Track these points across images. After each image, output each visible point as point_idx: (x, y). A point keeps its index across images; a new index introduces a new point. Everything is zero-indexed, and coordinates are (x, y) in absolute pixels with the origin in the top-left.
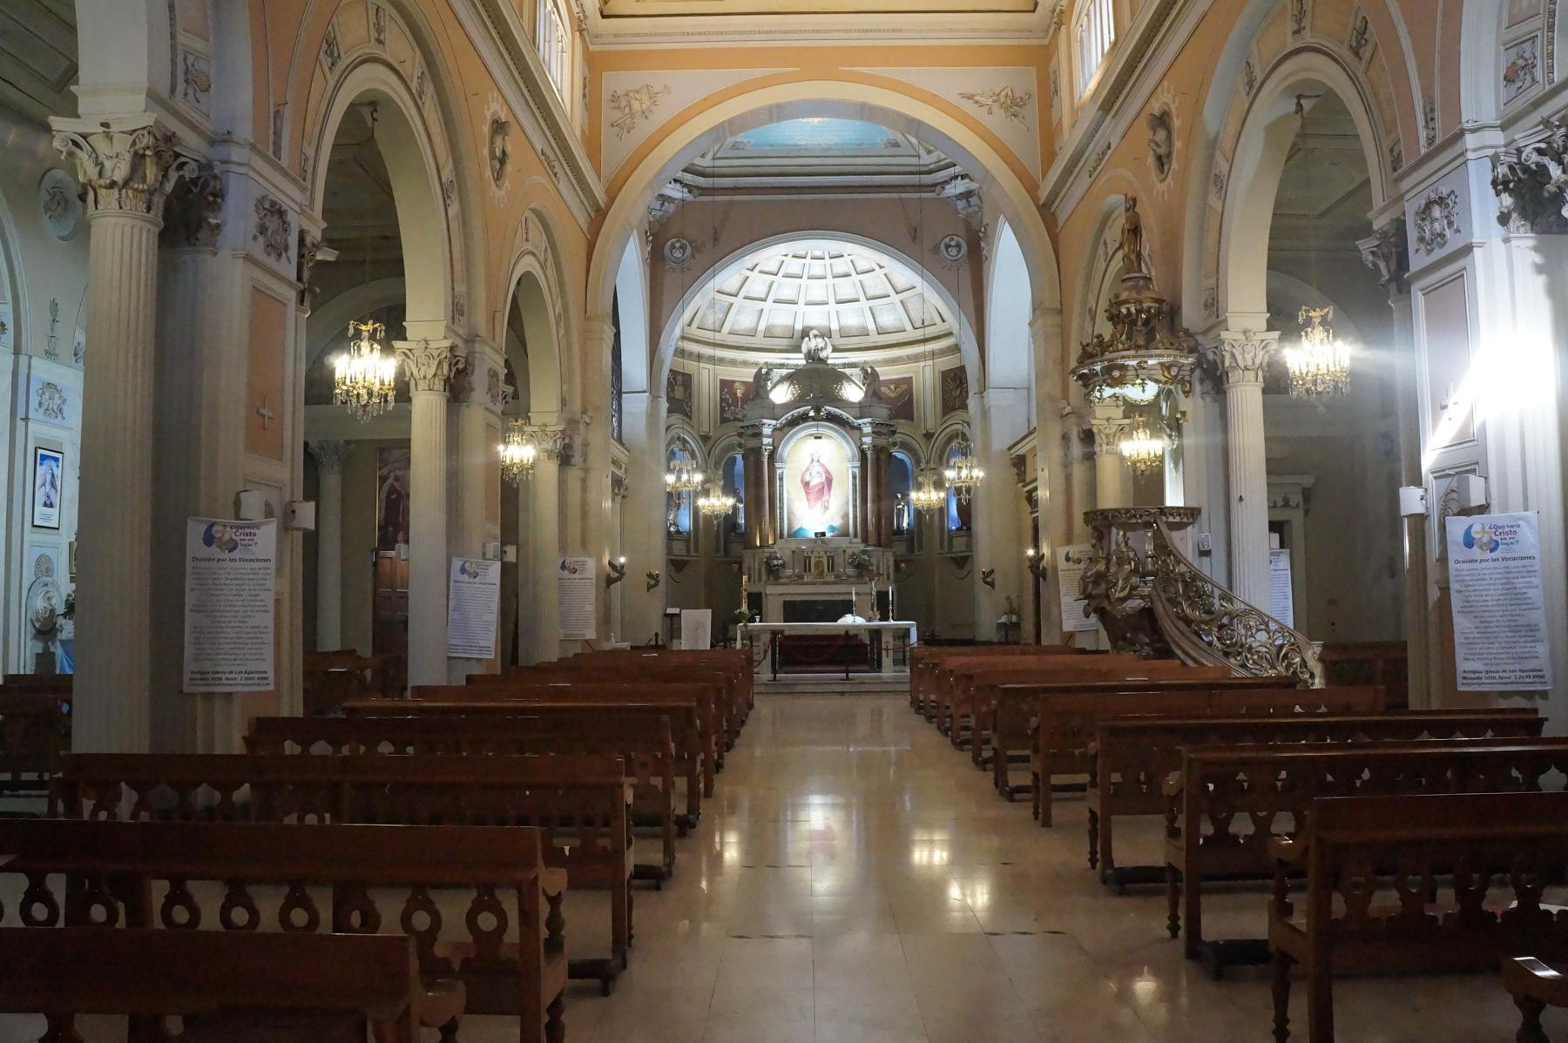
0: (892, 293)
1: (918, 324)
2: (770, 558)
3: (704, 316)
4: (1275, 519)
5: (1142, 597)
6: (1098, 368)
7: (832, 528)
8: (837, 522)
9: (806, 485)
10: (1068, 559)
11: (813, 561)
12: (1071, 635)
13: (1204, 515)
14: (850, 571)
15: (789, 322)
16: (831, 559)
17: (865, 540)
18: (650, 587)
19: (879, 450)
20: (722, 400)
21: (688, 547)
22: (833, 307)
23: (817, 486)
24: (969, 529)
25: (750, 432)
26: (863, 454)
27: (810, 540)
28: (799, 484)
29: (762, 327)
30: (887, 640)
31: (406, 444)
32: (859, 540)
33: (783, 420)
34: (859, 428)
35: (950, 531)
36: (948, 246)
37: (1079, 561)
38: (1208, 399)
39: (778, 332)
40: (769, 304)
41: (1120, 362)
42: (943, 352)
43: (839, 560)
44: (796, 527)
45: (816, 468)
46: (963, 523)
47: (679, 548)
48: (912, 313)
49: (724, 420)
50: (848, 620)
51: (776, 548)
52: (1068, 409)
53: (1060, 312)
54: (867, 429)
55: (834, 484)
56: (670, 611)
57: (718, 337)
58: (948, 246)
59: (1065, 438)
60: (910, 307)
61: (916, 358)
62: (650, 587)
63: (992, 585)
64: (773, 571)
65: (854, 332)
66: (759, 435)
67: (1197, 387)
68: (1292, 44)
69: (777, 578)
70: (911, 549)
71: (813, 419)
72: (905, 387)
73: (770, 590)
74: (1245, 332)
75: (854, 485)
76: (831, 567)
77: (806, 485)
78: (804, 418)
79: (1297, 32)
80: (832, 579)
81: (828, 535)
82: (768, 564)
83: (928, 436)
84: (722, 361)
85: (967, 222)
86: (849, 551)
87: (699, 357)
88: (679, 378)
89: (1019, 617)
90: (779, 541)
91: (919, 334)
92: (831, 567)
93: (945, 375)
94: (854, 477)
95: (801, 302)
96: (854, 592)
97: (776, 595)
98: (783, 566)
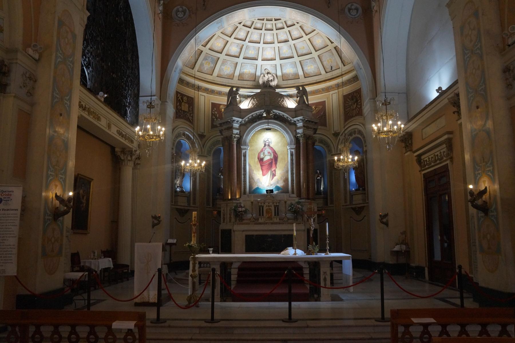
0: (313, 51)
1: (329, 70)
2: (236, 207)
3: (202, 64)
4: (244, 250)
7: (277, 188)
8: (281, 184)
9: (261, 160)
11: (265, 209)
14: (289, 215)
15: (252, 71)
16: (277, 207)
17: (299, 195)
18: (154, 226)
19: (307, 137)
20: (212, 114)
21: (189, 201)
22: (278, 62)
23: (268, 160)
24: (364, 189)
25: (225, 127)
26: (297, 140)
27: (264, 195)
28: (257, 160)
29: (237, 73)
30: (325, 270)
32: (295, 195)
33: (246, 119)
34: (295, 124)
35: (350, 191)
36: (349, 10)
39: (246, 77)
40: (240, 60)
42: (344, 84)
43: (282, 208)
44: (255, 187)
45: (268, 150)
46: (359, 186)
47: (182, 202)
48: (325, 63)
49: (213, 126)
50: (290, 252)
51: (241, 201)
54: (300, 124)
55: (279, 159)
56: (170, 241)
57: (209, 78)
58: (349, 10)
60: (324, 59)
61: (328, 89)
62: (154, 226)
63: (387, 224)
64: (239, 215)
65: (291, 77)
66: (231, 128)
69: (241, 219)
70: (326, 204)
71: (265, 118)
72: (321, 107)
73: (236, 227)
75: (292, 160)
76: (277, 213)
77: (261, 160)
78: (260, 117)
80: (278, 220)
81: (275, 192)
82: (235, 210)
83: (336, 135)
84: (212, 92)
86: (289, 203)
87: (199, 88)
88: (185, 98)
90: (243, 196)
91: (329, 75)
92: (277, 213)
93: (346, 98)
94: (292, 155)
95: (260, 59)
96: (295, 229)
97: (240, 232)
98: (245, 212)
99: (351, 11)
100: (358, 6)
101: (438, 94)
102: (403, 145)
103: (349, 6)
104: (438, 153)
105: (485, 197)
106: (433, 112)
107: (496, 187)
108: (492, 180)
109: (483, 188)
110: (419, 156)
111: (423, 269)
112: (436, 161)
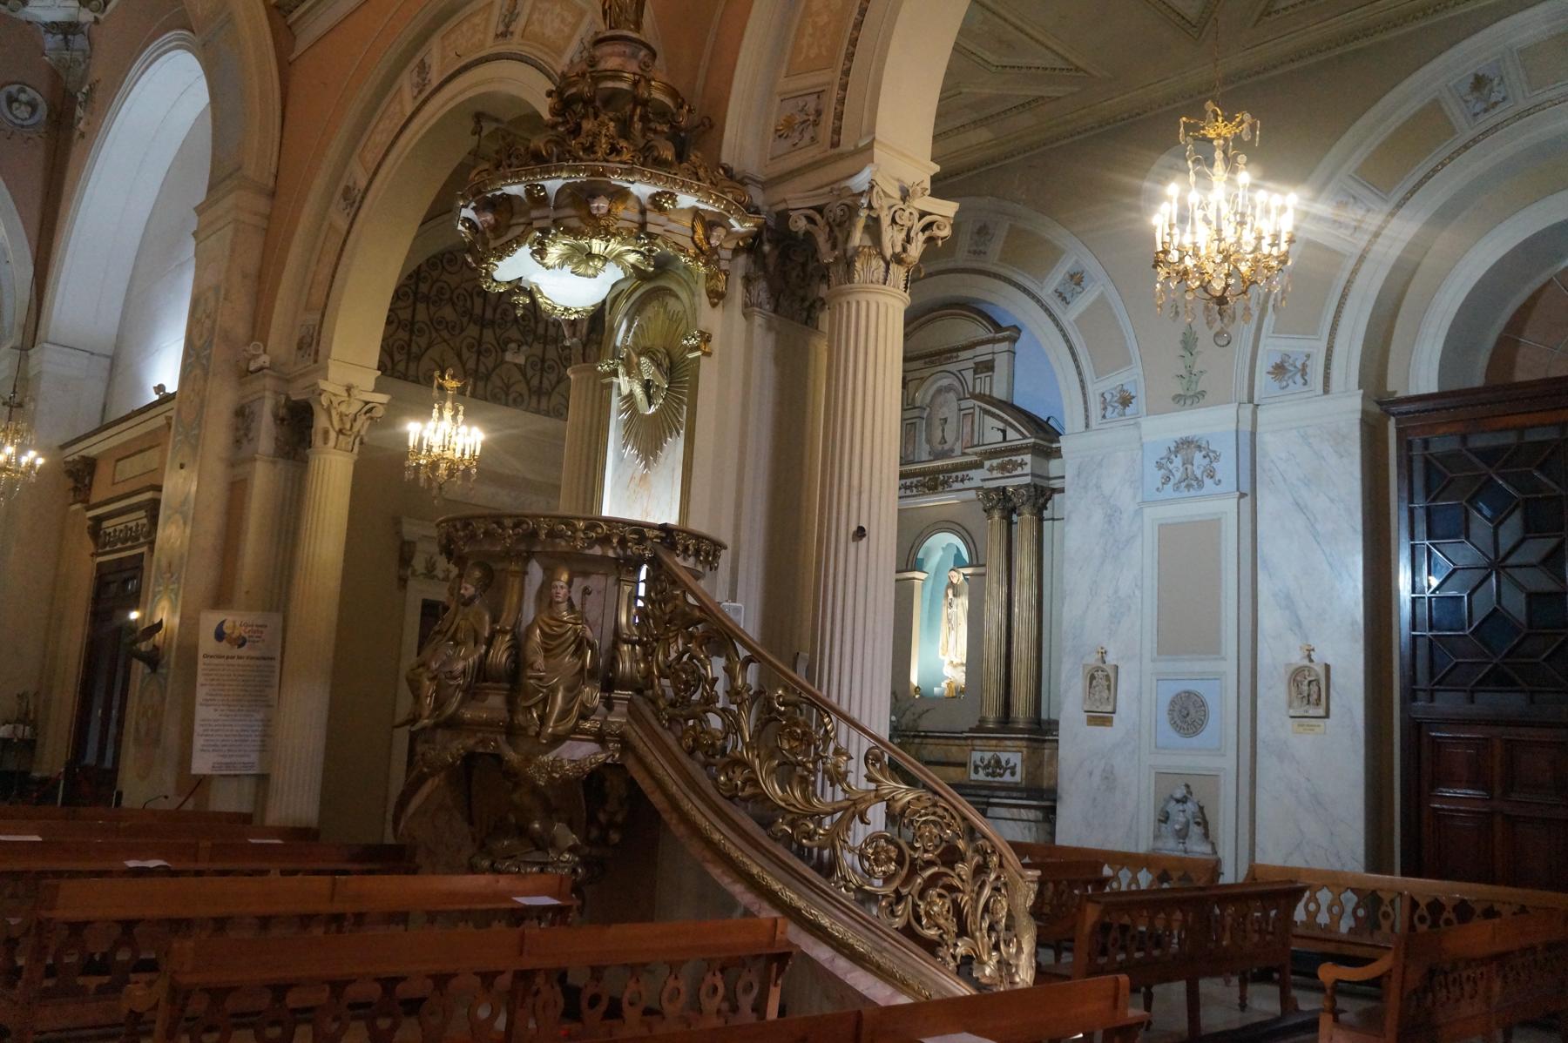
5: (600, 738)
6: (553, 185)
10: (220, 635)
12: (202, 782)
13: (725, 558)
31: (414, 871)
37: (241, 642)
38: (758, 320)
41: (616, 180)
52: (265, 360)
53: (273, 195)
59: (243, 416)
67: (738, 292)
68: (490, 48)
74: (349, 389)
79: (504, 35)
85: (55, 75)
89: (35, 728)
99: (15, 105)
100: (39, 98)
101: (156, 397)
102: (70, 483)
103: (14, 88)
104: (133, 524)
105: (158, 637)
106: (126, 436)
107: (177, 620)
108: (173, 611)
109: (157, 621)
110: (98, 520)
111: (57, 781)
112: (126, 540)
